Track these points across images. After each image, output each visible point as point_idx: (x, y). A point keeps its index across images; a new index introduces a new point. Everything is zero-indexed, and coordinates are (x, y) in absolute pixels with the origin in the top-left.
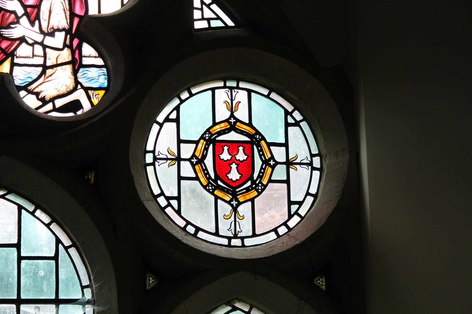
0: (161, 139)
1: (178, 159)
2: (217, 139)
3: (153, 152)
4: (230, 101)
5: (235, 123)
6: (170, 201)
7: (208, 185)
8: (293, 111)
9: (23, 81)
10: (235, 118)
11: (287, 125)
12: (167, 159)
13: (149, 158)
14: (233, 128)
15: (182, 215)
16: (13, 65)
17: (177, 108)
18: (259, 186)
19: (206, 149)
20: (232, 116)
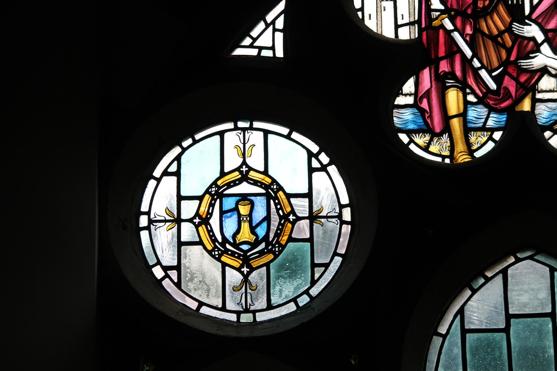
0: (159, 198)
1: (178, 221)
2: (225, 193)
3: (148, 213)
4: (242, 146)
5: (247, 172)
6: (168, 272)
7: (213, 250)
8: (319, 153)
9: (548, 120)
10: (247, 166)
11: (311, 170)
12: (165, 221)
13: (143, 221)
14: (245, 178)
15: (183, 288)
16: (535, 101)
17: (178, 158)
18: (275, 247)
19: (212, 205)
20: (244, 163)
